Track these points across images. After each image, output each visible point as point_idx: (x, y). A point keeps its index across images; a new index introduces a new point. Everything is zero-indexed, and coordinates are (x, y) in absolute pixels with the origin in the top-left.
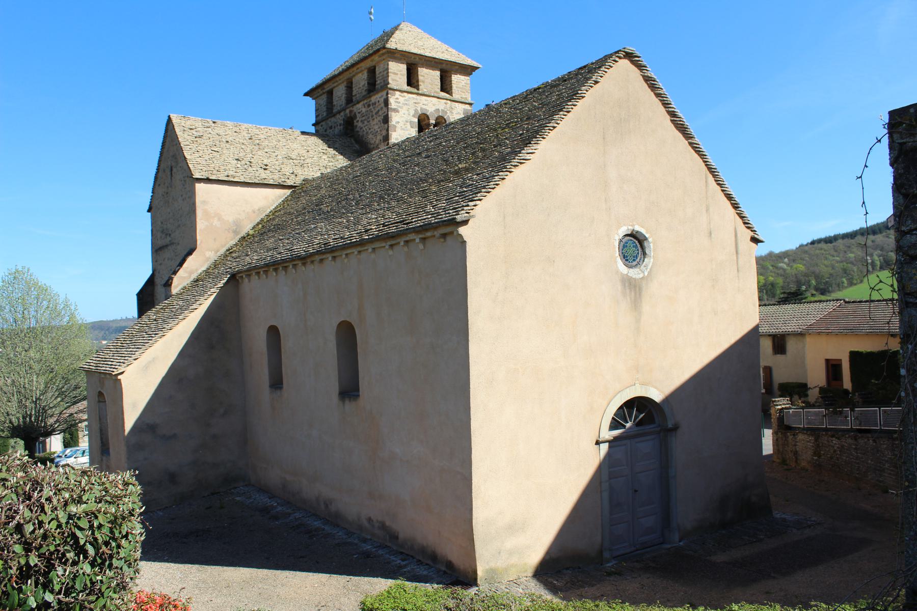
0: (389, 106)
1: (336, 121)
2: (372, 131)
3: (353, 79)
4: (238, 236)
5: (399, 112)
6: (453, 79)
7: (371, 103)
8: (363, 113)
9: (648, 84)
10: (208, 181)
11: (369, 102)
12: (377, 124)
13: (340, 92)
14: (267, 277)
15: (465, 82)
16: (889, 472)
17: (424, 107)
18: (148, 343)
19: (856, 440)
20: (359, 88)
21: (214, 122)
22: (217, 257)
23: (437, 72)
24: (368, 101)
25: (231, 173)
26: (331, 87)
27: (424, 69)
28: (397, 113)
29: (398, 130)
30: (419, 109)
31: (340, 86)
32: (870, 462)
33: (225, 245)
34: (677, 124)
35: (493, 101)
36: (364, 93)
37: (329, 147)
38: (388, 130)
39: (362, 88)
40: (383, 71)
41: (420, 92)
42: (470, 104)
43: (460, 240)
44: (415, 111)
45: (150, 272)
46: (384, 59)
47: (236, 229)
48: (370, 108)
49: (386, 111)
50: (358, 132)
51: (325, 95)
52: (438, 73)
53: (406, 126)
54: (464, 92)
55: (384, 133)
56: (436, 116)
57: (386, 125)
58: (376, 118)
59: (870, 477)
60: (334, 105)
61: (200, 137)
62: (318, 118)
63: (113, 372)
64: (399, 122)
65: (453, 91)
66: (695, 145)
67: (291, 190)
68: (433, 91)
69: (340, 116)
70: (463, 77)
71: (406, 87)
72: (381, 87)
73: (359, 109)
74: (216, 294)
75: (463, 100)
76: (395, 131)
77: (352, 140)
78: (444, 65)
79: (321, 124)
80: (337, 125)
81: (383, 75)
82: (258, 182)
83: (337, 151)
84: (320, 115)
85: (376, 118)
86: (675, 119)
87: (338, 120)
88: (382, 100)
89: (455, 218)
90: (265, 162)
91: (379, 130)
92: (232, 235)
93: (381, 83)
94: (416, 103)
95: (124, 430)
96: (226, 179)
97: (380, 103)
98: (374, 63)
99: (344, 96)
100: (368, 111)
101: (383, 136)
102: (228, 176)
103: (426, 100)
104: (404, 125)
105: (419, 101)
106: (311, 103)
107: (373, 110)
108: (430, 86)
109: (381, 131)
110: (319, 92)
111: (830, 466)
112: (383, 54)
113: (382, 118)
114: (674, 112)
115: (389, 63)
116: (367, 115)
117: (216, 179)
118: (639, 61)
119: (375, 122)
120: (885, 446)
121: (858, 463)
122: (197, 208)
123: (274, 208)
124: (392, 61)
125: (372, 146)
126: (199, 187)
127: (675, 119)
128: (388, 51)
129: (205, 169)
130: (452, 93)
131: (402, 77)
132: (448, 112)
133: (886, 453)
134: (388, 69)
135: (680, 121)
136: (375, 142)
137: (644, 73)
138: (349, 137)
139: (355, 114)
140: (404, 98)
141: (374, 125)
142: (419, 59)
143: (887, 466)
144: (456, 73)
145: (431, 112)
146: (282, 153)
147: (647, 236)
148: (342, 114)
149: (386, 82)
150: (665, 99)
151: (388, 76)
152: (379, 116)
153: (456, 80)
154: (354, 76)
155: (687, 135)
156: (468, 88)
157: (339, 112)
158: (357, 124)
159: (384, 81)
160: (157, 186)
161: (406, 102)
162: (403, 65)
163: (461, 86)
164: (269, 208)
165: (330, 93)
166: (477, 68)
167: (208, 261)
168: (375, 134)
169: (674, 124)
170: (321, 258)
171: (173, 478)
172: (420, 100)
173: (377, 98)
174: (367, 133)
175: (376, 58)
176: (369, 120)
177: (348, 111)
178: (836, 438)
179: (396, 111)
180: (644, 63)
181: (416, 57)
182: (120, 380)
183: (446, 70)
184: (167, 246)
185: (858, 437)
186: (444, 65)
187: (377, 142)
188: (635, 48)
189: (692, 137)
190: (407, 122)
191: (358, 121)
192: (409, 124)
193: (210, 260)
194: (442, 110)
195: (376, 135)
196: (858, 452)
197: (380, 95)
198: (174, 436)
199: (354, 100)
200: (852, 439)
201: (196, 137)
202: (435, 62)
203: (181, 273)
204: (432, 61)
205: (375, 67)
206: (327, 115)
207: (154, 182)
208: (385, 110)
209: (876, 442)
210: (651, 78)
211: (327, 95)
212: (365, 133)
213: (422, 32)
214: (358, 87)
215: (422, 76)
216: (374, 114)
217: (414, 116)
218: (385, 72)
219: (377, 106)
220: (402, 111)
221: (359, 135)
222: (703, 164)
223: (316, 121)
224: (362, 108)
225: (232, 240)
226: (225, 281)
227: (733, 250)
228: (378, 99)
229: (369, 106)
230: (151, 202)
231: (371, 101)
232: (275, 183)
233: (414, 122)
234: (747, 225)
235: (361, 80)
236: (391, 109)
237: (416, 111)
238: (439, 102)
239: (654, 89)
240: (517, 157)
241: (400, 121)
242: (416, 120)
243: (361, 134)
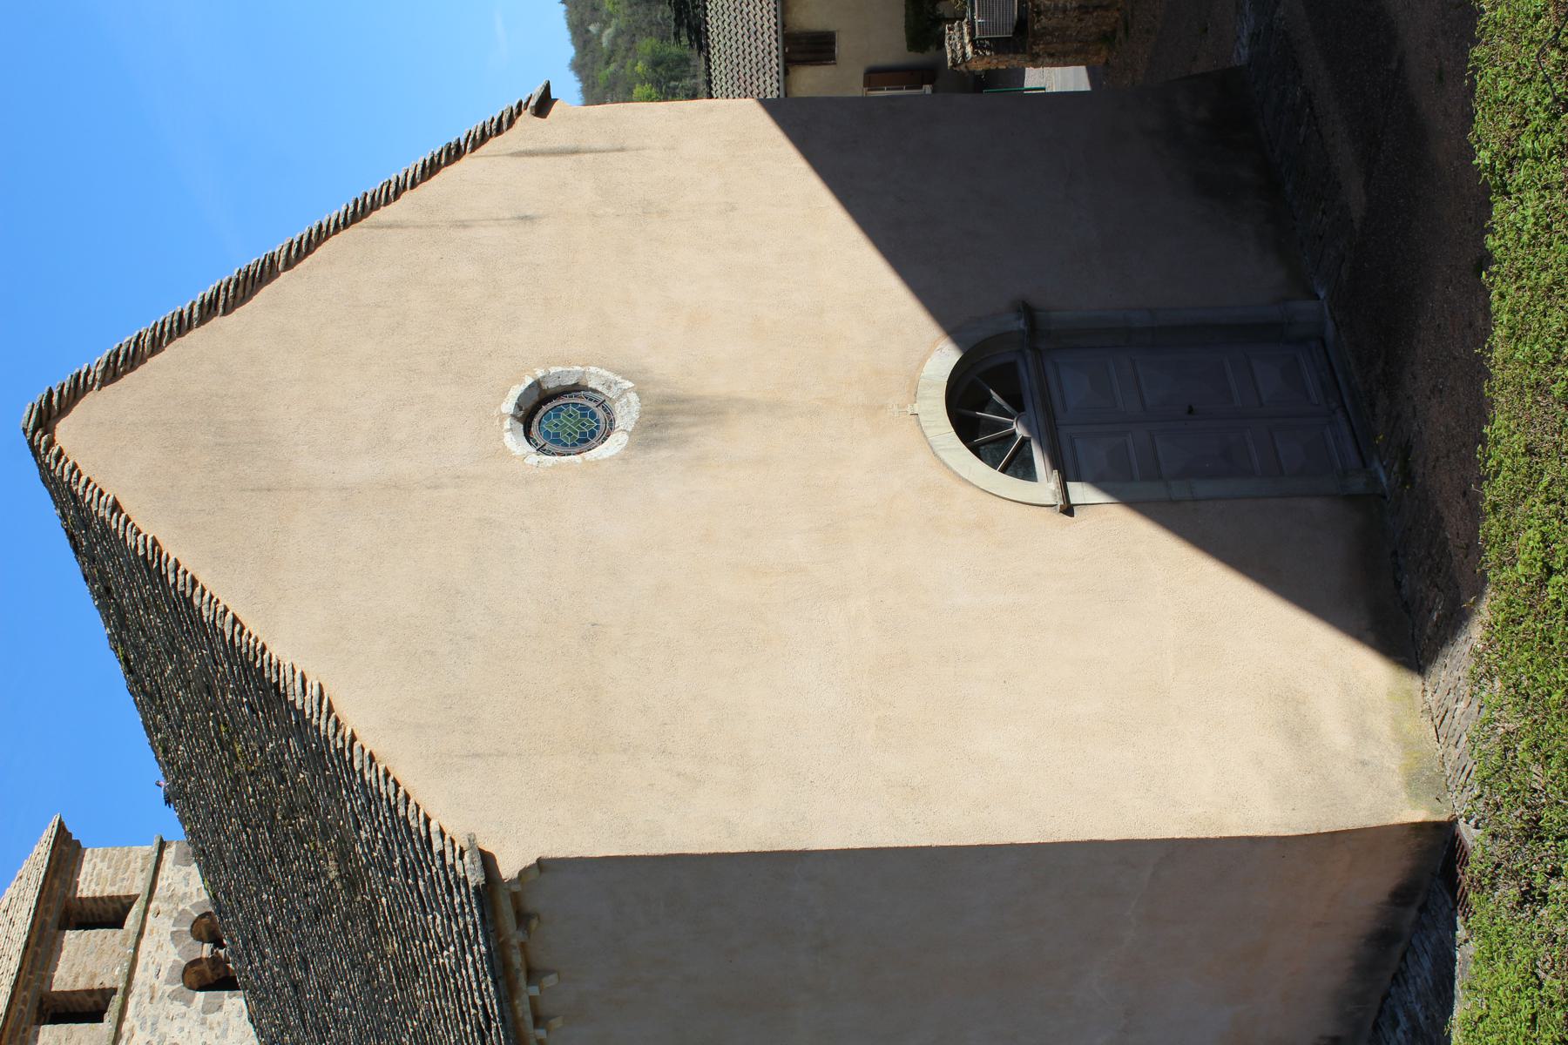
6: (90, 895)
9: (125, 372)
17: (164, 974)
30: (169, 988)
34: (235, 297)
41: (121, 985)
42: (162, 846)
54: (128, 864)
70: (86, 867)
71: (106, 1027)
75: (150, 866)
78: (49, 919)
86: (221, 303)
94: (152, 998)
118: (61, 393)
127: (221, 303)
130: (128, 897)
135: (227, 289)
140: (137, 1032)
147: (529, 381)
150: (167, 328)
156: (115, 852)
189: (272, 260)
192: (210, 1017)
202: (38, 944)
204: (36, 953)
210: (108, 362)
217: (188, 1003)
237: (173, 997)
238: (151, 931)
239: (139, 356)
240: (314, 721)
242: (200, 995)
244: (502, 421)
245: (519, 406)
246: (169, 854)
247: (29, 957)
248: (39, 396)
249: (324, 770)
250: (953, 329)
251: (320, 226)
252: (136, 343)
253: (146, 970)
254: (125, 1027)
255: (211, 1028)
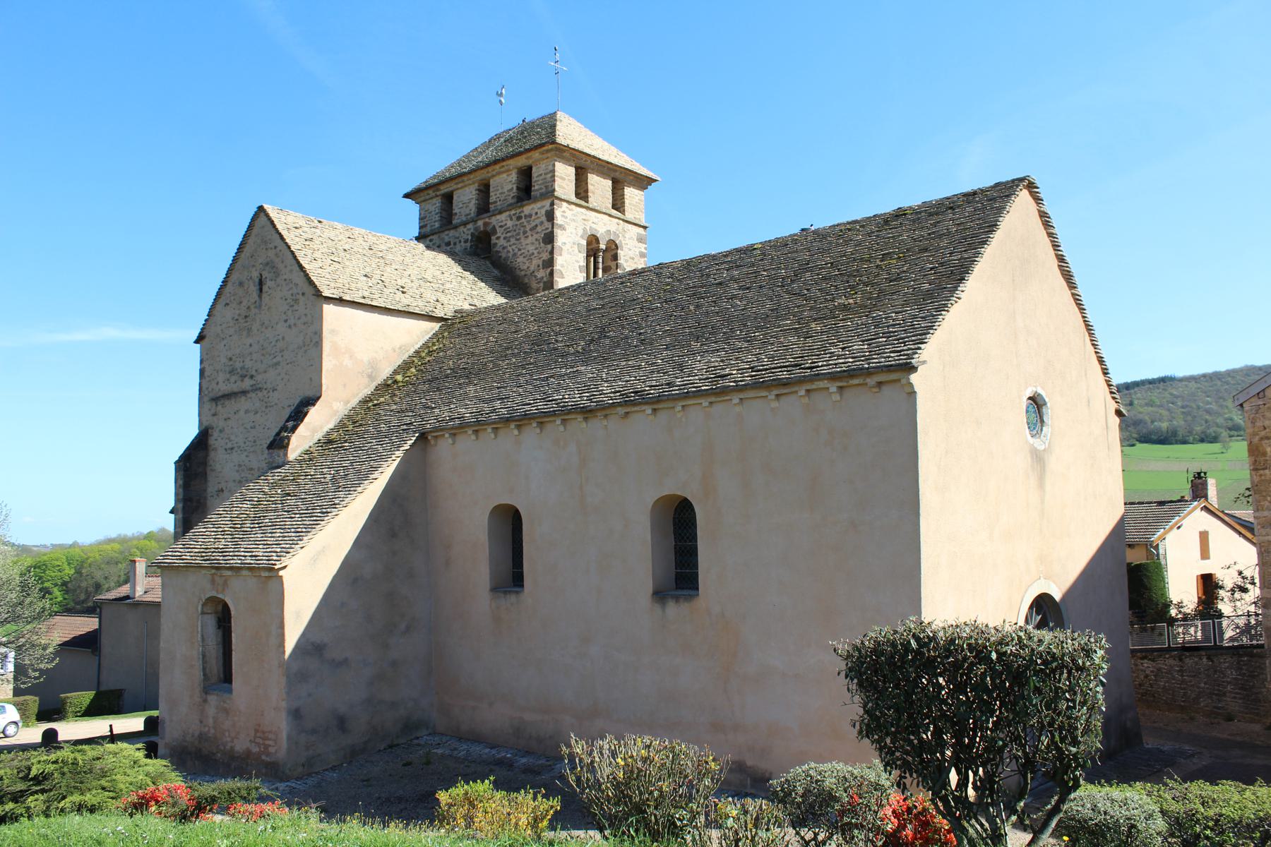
2: (524, 253)
4: (374, 383)
5: (565, 230)
6: (625, 193)
8: (509, 228)
9: (1042, 221)
10: (340, 301)
12: (533, 243)
13: (466, 199)
14: (477, 438)
16: (1233, 695)
17: (594, 226)
18: (319, 524)
19: (1181, 660)
21: (320, 222)
22: (348, 411)
23: (608, 181)
26: (451, 189)
27: (595, 176)
30: (588, 228)
31: (467, 189)
32: (1202, 685)
33: (357, 395)
34: (1064, 270)
35: (812, 225)
36: (511, 201)
38: (552, 252)
41: (591, 206)
42: (645, 228)
43: (910, 390)
45: (192, 432)
46: (547, 158)
47: (372, 373)
48: (521, 221)
49: (550, 226)
51: (440, 197)
54: (637, 212)
55: (545, 256)
57: (549, 247)
58: (532, 235)
59: (1202, 704)
60: (456, 214)
61: (311, 240)
63: (275, 565)
64: (565, 243)
66: (1077, 297)
67: (440, 324)
70: (636, 192)
71: (573, 198)
74: (399, 459)
75: (637, 222)
76: (561, 255)
78: (617, 174)
79: (431, 237)
82: (402, 309)
85: (532, 235)
86: (1063, 264)
88: (543, 212)
89: (911, 363)
90: (400, 282)
91: (535, 252)
92: (366, 380)
93: (541, 189)
94: (584, 220)
95: (285, 651)
97: (539, 215)
98: (530, 162)
99: (474, 202)
101: (543, 261)
102: (364, 298)
106: (413, 208)
107: (525, 224)
109: (538, 253)
110: (428, 194)
111: (1139, 696)
113: (542, 236)
114: (1062, 256)
115: (556, 163)
116: (515, 231)
117: (352, 300)
118: (1038, 193)
119: (530, 240)
120: (1227, 665)
121: (1184, 689)
122: (324, 340)
123: (419, 346)
125: (523, 273)
127: (1063, 264)
129: (333, 285)
130: (624, 211)
131: (569, 183)
132: (620, 235)
133: (1229, 672)
134: (553, 171)
135: (1067, 267)
137: (1040, 207)
138: (483, 258)
139: (494, 227)
140: (571, 212)
141: (527, 244)
143: (1229, 688)
144: (631, 184)
146: (413, 271)
147: (1047, 400)
148: (470, 226)
149: (550, 189)
150: (1056, 240)
151: (554, 181)
154: (493, 176)
155: (1071, 284)
156: (642, 206)
157: (465, 224)
158: (497, 241)
159: (546, 187)
160: (219, 307)
164: (413, 346)
165: (448, 198)
167: (335, 415)
168: (530, 257)
169: (1060, 270)
170: (627, 411)
171: (342, 723)
173: (535, 208)
174: (515, 255)
176: (518, 237)
177: (480, 223)
178: (1150, 659)
180: (1041, 196)
181: (588, 158)
182: (281, 576)
183: (620, 179)
184: (244, 393)
185: (1183, 657)
186: (617, 174)
188: (661, 178)
189: (1075, 288)
190: (574, 243)
191: (498, 238)
192: (576, 246)
193: (338, 414)
196: (1185, 674)
197: (539, 205)
198: (345, 662)
199: (491, 209)
200: (1174, 659)
201: (306, 240)
202: (608, 168)
203: (302, 429)
204: (604, 167)
205: (530, 168)
207: (215, 300)
209: (1212, 661)
210: (1047, 214)
211: (441, 199)
212: (510, 255)
213: (583, 126)
215: (592, 185)
216: (528, 230)
217: (582, 237)
218: (550, 175)
219: (535, 219)
220: (570, 229)
222: (1081, 320)
223: (419, 233)
224: (507, 220)
225: (366, 388)
226: (412, 441)
227: (1104, 424)
228: (536, 210)
229: (519, 218)
230: (202, 329)
231: (523, 212)
234: (1113, 395)
235: (504, 184)
236: (557, 224)
237: (584, 230)
238: (611, 221)
239: (1047, 227)
240: (955, 295)
241: (567, 242)
242: (584, 243)
243: (504, 255)
244: (1034, 386)
245: (1039, 395)
246: (641, 231)
247: (603, 163)
248: (1038, 183)
249: (923, 299)
250: (1068, 595)
251: (1085, 310)
252: (1052, 226)
253: (595, 217)
254: (573, 207)
255: (572, 247)
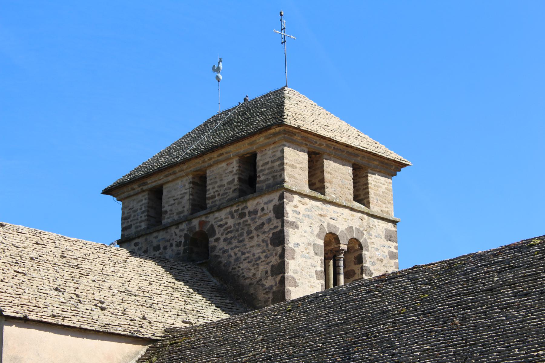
0: (285, 218)
1: (168, 237)
3: (208, 171)
6: (369, 181)
7: (246, 211)
8: (230, 227)
11: (243, 209)
12: (259, 246)
15: (386, 186)
17: (332, 222)
20: (220, 187)
24: (240, 207)
25: (57, 311)
26: (160, 182)
27: (332, 162)
28: (296, 230)
29: (298, 256)
30: (325, 225)
31: (179, 182)
36: (232, 195)
37: (177, 280)
38: (282, 256)
39: (226, 186)
40: (273, 162)
41: (328, 198)
42: (394, 222)
44: (321, 228)
48: (244, 219)
49: (280, 224)
50: (217, 257)
51: (147, 193)
52: (350, 170)
53: (308, 251)
54: (385, 203)
55: (274, 260)
56: (349, 238)
57: (279, 249)
58: (258, 236)
60: (166, 212)
62: (127, 233)
64: (298, 244)
65: (371, 199)
67: (147, 347)
68: (344, 198)
69: (177, 231)
70: (383, 179)
71: (306, 190)
72: (269, 187)
73: (222, 220)
76: (293, 258)
77: (205, 270)
79: (136, 241)
80: (171, 245)
81: (273, 167)
82: (101, 330)
83: (190, 287)
84: (133, 227)
85: (258, 236)
87: (174, 236)
88: (271, 207)
91: (263, 256)
93: (268, 179)
94: (321, 215)
96: (51, 320)
99: (187, 197)
100: (239, 224)
102: (54, 316)
103: (334, 212)
104: (306, 249)
105: (325, 212)
108: (339, 189)
109: (266, 257)
110: (133, 189)
112: (275, 134)
113: (271, 235)
119: (255, 242)
124: (289, 147)
125: (248, 282)
126: (9, 331)
128: (284, 130)
129: (16, 302)
130: (368, 203)
131: (301, 172)
132: (365, 232)
134: (282, 158)
136: (254, 275)
140: (304, 207)
141: (252, 247)
142: (327, 145)
145: (342, 231)
146: (115, 283)
148: (183, 226)
149: (279, 179)
151: (283, 170)
152: (264, 232)
153: (374, 183)
154: (211, 166)
156: (390, 196)
157: (177, 224)
158: (216, 244)
161: (309, 213)
162: (302, 153)
163: (381, 193)
166: (406, 165)
168: (256, 262)
172: (328, 211)
174: (237, 259)
175: (261, 139)
177: (195, 222)
179: (294, 225)
187: (259, 275)
191: (217, 240)
192: (311, 248)
194: (356, 228)
195: (257, 264)
197: (265, 198)
202: (348, 152)
204: (343, 151)
206: (148, 228)
208: (275, 225)
211: (148, 194)
214: (218, 184)
217: (318, 236)
218: (278, 163)
221: (220, 262)
228: (262, 206)
229: (242, 215)
231: (247, 208)
232: (125, 333)
233: (319, 246)
236: (288, 222)
237: (321, 227)
238: (353, 216)
241: (300, 243)
242: (321, 243)
243: (224, 260)
